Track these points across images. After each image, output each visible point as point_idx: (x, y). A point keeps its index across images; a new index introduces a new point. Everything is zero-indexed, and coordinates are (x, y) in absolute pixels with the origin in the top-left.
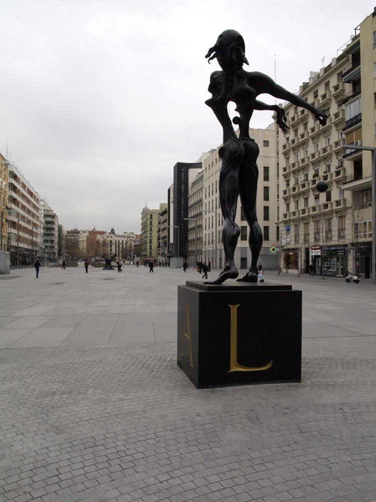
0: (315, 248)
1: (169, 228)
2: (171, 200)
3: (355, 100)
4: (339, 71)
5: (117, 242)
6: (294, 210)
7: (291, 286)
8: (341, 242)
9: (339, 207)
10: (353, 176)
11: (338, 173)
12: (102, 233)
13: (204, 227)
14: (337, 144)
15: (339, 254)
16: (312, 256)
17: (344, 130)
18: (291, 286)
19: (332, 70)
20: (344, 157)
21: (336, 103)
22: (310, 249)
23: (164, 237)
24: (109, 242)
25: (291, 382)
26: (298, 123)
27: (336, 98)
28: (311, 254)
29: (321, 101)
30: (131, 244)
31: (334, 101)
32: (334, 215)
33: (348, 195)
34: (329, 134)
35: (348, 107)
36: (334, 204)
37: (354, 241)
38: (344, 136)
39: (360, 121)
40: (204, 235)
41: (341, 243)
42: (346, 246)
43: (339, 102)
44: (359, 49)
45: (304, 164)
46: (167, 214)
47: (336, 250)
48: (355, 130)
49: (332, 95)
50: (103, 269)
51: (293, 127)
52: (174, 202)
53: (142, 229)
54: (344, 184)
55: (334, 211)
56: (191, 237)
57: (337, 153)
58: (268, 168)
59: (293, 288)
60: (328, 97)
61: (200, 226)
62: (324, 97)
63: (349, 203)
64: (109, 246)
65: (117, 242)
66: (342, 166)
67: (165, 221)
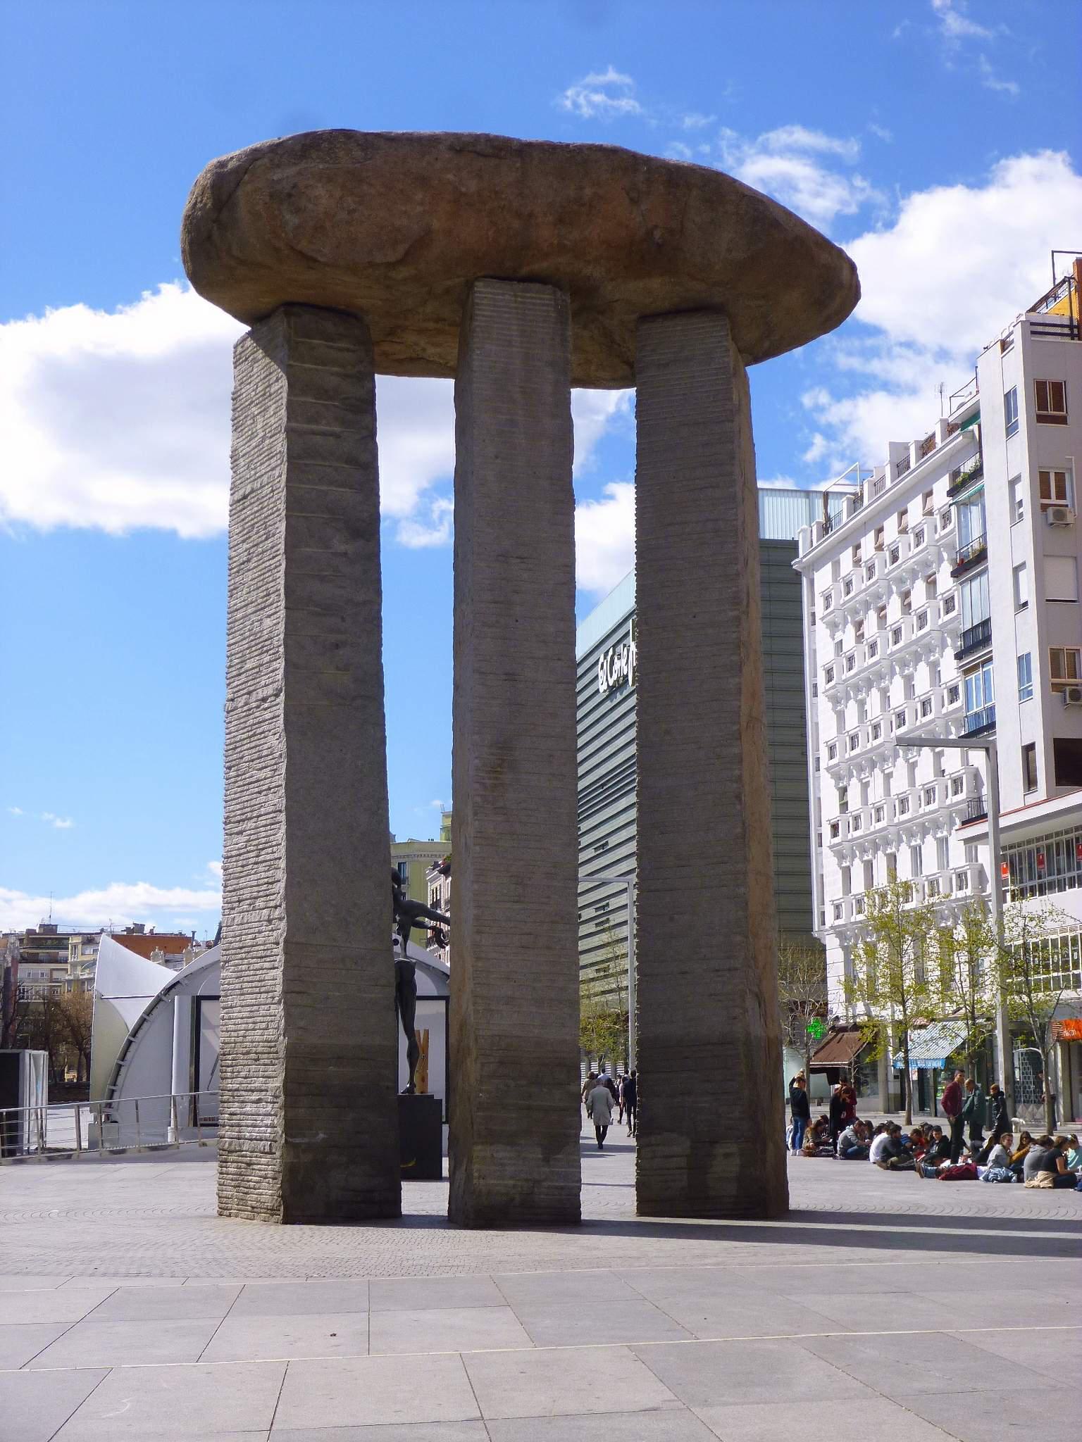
33: (985, 855)
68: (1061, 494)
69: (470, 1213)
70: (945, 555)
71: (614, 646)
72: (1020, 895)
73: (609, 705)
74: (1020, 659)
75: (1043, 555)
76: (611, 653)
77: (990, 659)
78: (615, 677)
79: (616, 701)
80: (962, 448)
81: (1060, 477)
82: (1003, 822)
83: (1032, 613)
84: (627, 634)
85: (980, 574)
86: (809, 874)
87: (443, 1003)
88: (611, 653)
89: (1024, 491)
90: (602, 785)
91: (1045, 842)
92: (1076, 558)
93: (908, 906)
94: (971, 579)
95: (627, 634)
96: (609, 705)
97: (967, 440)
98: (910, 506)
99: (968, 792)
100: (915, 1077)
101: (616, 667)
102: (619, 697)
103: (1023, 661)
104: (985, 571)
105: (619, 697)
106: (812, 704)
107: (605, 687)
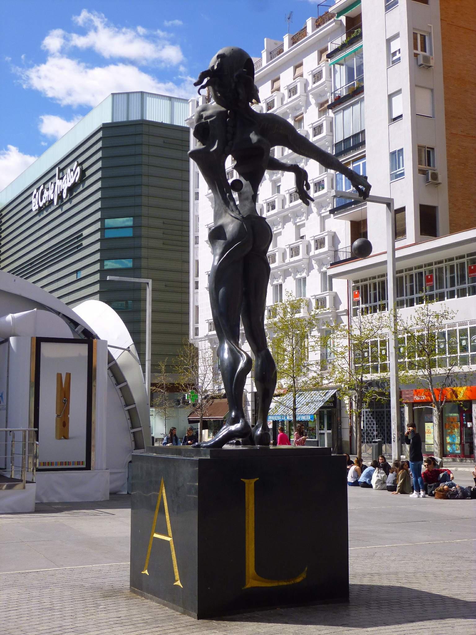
33: (341, 287)
35: (340, 116)
39: (363, 143)
68: (424, 49)
69: (471, 421)
70: (312, 101)
71: (44, 184)
72: (365, 312)
73: (37, 218)
74: (393, 154)
75: (415, 86)
76: (42, 188)
77: (364, 157)
78: (44, 201)
79: (42, 216)
80: (335, 30)
81: (423, 38)
82: (398, 254)
83: (406, 124)
84: (55, 176)
85: (356, 103)
86: (188, 303)
87: (45, 348)
88: (42, 188)
89: (402, 45)
90: (31, 264)
91: (372, 281)
92: (432, 90)
93: (297, 316)
94: (344, 109)
95: (55, 176)
96: (37, 218)
97: (337, 26)
98: (282, 75)
99: (329, 247)
100: (270, 426)
101: (46, 194)
102: (45, 213)
103: (396, 156)
104: (362, 100)
105: (45, 213)
106: (194, 204)
107: (37, 207)
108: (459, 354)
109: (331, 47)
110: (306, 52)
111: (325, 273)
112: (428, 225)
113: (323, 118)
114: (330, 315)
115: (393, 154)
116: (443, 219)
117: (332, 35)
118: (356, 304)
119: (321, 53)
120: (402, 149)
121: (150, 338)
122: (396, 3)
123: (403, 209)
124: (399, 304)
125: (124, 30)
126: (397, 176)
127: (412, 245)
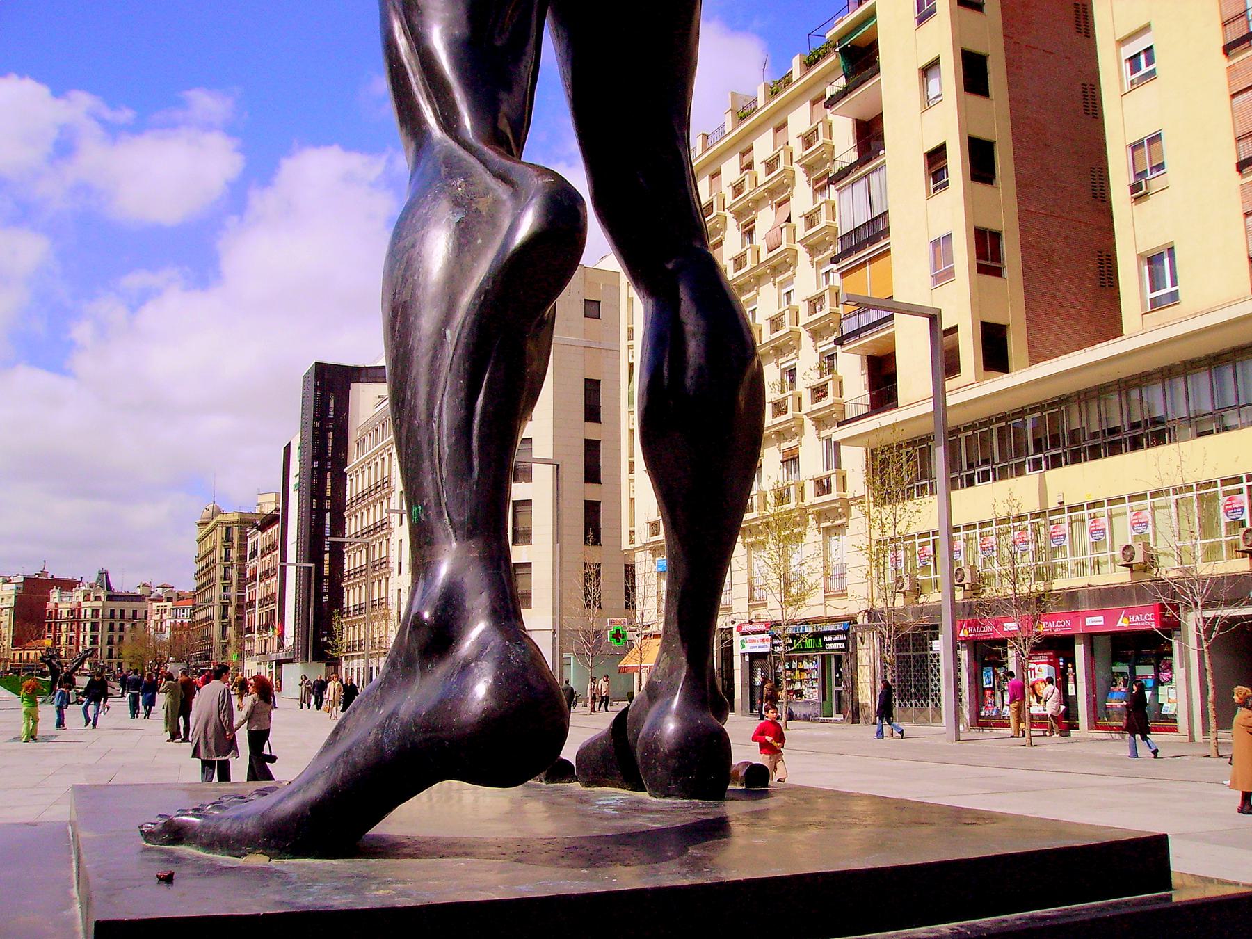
0: (752, 628)
1: (283, 569)
2: (294, 481)
3: (853, 183)
4: (815, 93)
5: (117, 613)
6: (820, 472)
7: (1156, 847)
8: (835, 609)
9: (826, 498)
10: (867, 400)
11: (819, 392)
12: (68, 585)
13: (394, 565)
14: (814, 303)
15: (828, 646)
16: (743, 655)
17: (835, 260)
18: (1156, 847)
19: (727, 139)
20: (839, 342)
21: (808, 181)
22: (735, 633)
23: (265, 599)
24: (89, 612)
25: (303, 805)
26: (757, 203)
27: (809, 169)
28: (737, 650)
29: (762, 178)
30: (162, 621)
31: (801, 177)
32: (812, 522)
33: (854, 460)
34: (789, 273)
35: (847, 194)
36: (810, 488)
37: (879, 604)
38: (836, 280)
39: (885, 232)
40: (393, 595)
41: (832, 613)
42: (852, 620)
43: (817, 181)
44: (874, 29)
45: (819, 315)
46: (278, 526)
47: (817, 635)
48: (870, 260)
49: (795, 160)
50: (373, 185)
51: (738, 215)
52: (300, 488)
53: (198, 576)
54: (839, 425)
55: (810, 511)
56: (351, 598)
57: (816, 334)
58: (597, 383)
59: (1181, 862)
60: (782, 165)
61: (383, 563)
62: (771, 165)
63: (857, 483)
64: (88, 626)
65: (117, 613)
66: (831, 369)
67: (270, 549)
104: (883, 166)
108: (1223, 539)
109: (830, 91)
110: (792, 103)
111: (828, 440)
112: (995, 355)
113: (821, 199)
114: (838, 505)
115: (935, 243)
116: (1016, 345)
117: (825, 77)
118: (907, 472)
119: (814, 103)
120: (1151, 47)
121: (646, 380)
122: (932, 12)
123: (954, 329)
124: (953, 485)
125: (521, 589)
126: (942, 276)
127: (973, 388)
